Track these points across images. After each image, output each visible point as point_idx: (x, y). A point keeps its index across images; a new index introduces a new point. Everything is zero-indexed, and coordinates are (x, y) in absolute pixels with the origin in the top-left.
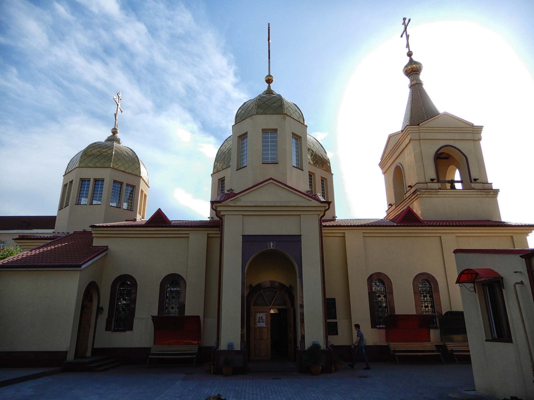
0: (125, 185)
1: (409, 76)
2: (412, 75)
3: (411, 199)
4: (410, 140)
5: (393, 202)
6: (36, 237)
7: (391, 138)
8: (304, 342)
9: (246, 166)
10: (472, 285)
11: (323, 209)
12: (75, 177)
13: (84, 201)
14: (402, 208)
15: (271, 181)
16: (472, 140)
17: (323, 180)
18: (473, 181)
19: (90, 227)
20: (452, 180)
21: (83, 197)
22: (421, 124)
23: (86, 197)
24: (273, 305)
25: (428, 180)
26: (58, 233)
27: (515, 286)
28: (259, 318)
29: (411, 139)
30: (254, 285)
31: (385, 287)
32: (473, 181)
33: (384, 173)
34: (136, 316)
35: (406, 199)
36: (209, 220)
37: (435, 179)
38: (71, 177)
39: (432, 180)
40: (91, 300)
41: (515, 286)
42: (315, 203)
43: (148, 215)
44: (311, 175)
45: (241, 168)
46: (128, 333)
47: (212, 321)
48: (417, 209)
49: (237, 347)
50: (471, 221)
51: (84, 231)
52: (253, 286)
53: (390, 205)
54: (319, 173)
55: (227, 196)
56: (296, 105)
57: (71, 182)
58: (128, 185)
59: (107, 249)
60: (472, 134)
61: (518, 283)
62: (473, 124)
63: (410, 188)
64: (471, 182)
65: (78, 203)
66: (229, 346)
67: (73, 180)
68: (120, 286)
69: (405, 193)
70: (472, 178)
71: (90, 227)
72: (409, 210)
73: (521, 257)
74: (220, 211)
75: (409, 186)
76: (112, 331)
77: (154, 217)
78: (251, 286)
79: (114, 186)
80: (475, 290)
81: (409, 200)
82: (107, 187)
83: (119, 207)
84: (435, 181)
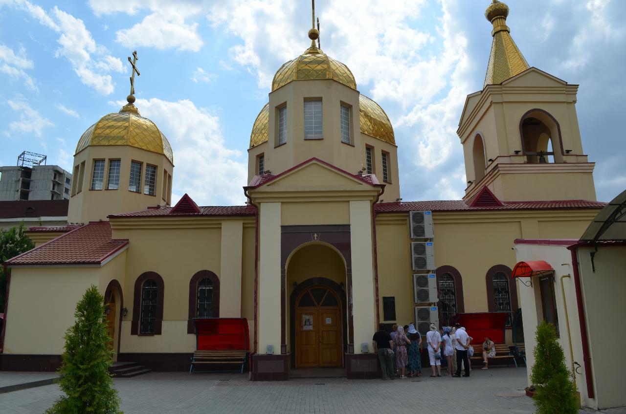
0: (144, 167)
1: (493, 21)
2: (498, 19)
3: (492, 176)
4: (491, 103)
5: (473, 179)
6: (44, 230)
7: (470, 99)
8: (353, 346)
9: (285, 143)
10: (528, 279)
11: (376, 194)
12: (88, 157)
13: (98, 186)
14: (480, 188)
15: (314, 162)
16: (566, 103)
17: (385, 154)
18: (565, 153)
19: (107, 217)
20: (541, 151)
21: (97, 180)
22: (503, 84)
23: (101, 181)
24: (322, 305)
25: (512, 152)
26: (72, 223)
27: (562, 279)
28: (306, 321)
29: (492, 101)
30: (299, 282)
31: (453, 283)
32: (565, 153)
33: (462, 142)
34: (186, 323)
35: (487, 175)
36: (246, 205)
37: (520, 151)
38: (83, 157)
39: (517, 152)
40: (113, 301)
41: (562, 279)
42: (366, 187)
43: (175, 200)
44: (369, 149)
45: (279, 146)
46: (156, 337)
47: (251, 323)
48: (500, 190)
49: (278, 351)
50: (560, 202)
51: (101, 222)
52: (298, 284)
53: (469, 182)
54: (379, 147)
55: (264, 180)
56: (345, 66)
57: (83, 164)
58: (148, 165)
59: (128, 243)
60: (565, 95)
61: (564, 277)
62: (567, 83)
63: (491, 162)
64: (563, 154)
65: (92, 189)
66: (268, 349)
67: (85, 161)
68: (144, 285)
69: (486, 167)
70: (565, 149)
71: (107, 217)
72: (486, 190)
73: (568, 248)
74: (256, 198)
75: (490, 160)
76: (139, 335)
77: (180, 204)
78: (295, 284)
79: (132, 167)
80: (531, 284)
81: (490, 178)
82: (125, 169)
83: (138, 192)
84: (520, 153)
